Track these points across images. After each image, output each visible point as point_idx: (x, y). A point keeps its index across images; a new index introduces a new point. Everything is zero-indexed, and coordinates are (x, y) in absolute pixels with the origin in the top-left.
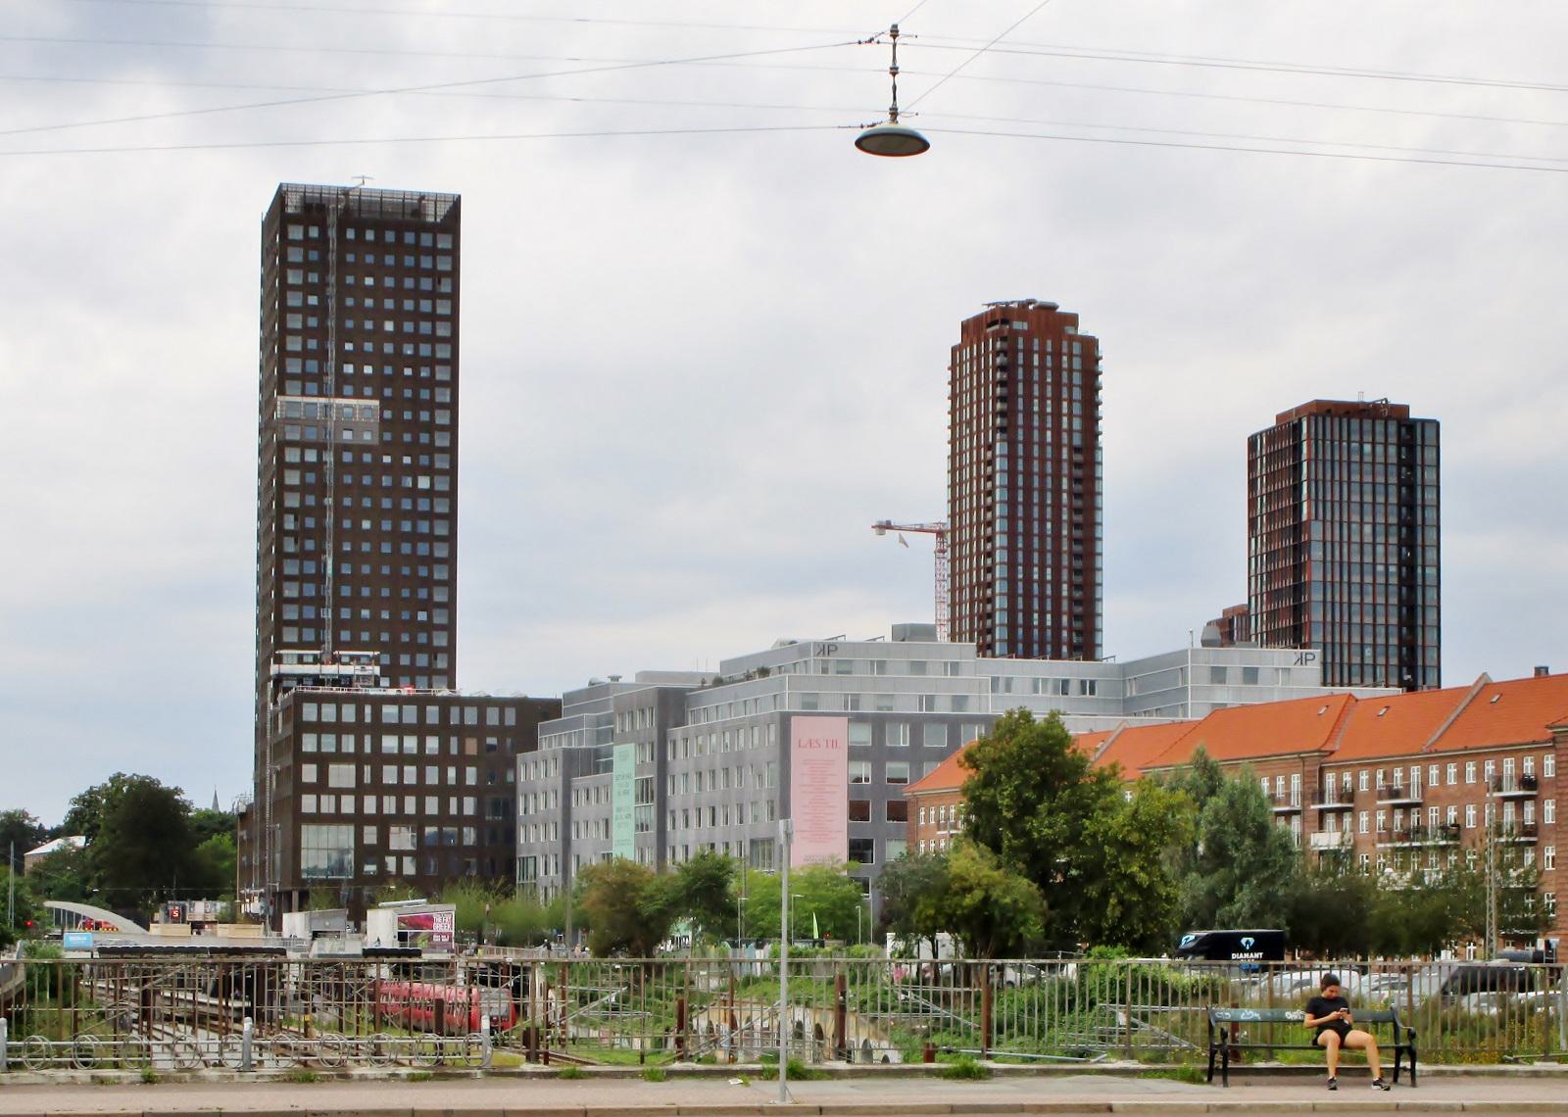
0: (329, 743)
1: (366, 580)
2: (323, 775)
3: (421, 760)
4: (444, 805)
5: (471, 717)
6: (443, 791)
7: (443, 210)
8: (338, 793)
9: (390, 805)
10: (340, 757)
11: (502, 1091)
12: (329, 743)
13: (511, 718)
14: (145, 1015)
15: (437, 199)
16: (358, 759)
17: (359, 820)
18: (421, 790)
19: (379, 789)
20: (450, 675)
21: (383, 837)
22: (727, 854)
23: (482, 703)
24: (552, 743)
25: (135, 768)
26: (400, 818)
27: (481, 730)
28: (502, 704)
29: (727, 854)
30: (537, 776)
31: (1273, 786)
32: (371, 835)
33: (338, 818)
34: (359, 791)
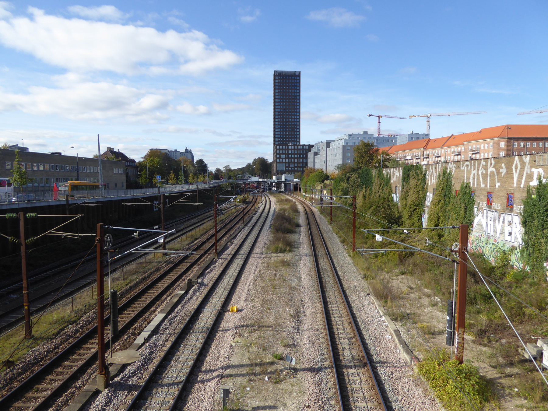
0: (281, 152)
1: (287, 128)
2: (280, 156)
3: (282, 149)
4: (298, 160)
5: (301, 147)
6: (297, 158)
7: (298, 73)
8: (282, 159)
9: (290, 161)
10: (283, 154)
11: (210, 303)
12: (281, 152)
13: (307, 147)
14: (366, 164)
15: (297, 72)
16: (285, 154)
17: (285, 163)
18: (294, 158)
19: (288, 158)
20: (299, 141)
21: (289, 165)
22: (220, 331)
23: (304, 145)
24: (313, 150)
25: (261, 156)
26: (291, 162)
27: (303, 149)
28: (306, 145)
29: (220, 331)
30: (310, 155)
31: (484, 147)
32: (287, 165)
33: (282, 162)
34: (285, 159)
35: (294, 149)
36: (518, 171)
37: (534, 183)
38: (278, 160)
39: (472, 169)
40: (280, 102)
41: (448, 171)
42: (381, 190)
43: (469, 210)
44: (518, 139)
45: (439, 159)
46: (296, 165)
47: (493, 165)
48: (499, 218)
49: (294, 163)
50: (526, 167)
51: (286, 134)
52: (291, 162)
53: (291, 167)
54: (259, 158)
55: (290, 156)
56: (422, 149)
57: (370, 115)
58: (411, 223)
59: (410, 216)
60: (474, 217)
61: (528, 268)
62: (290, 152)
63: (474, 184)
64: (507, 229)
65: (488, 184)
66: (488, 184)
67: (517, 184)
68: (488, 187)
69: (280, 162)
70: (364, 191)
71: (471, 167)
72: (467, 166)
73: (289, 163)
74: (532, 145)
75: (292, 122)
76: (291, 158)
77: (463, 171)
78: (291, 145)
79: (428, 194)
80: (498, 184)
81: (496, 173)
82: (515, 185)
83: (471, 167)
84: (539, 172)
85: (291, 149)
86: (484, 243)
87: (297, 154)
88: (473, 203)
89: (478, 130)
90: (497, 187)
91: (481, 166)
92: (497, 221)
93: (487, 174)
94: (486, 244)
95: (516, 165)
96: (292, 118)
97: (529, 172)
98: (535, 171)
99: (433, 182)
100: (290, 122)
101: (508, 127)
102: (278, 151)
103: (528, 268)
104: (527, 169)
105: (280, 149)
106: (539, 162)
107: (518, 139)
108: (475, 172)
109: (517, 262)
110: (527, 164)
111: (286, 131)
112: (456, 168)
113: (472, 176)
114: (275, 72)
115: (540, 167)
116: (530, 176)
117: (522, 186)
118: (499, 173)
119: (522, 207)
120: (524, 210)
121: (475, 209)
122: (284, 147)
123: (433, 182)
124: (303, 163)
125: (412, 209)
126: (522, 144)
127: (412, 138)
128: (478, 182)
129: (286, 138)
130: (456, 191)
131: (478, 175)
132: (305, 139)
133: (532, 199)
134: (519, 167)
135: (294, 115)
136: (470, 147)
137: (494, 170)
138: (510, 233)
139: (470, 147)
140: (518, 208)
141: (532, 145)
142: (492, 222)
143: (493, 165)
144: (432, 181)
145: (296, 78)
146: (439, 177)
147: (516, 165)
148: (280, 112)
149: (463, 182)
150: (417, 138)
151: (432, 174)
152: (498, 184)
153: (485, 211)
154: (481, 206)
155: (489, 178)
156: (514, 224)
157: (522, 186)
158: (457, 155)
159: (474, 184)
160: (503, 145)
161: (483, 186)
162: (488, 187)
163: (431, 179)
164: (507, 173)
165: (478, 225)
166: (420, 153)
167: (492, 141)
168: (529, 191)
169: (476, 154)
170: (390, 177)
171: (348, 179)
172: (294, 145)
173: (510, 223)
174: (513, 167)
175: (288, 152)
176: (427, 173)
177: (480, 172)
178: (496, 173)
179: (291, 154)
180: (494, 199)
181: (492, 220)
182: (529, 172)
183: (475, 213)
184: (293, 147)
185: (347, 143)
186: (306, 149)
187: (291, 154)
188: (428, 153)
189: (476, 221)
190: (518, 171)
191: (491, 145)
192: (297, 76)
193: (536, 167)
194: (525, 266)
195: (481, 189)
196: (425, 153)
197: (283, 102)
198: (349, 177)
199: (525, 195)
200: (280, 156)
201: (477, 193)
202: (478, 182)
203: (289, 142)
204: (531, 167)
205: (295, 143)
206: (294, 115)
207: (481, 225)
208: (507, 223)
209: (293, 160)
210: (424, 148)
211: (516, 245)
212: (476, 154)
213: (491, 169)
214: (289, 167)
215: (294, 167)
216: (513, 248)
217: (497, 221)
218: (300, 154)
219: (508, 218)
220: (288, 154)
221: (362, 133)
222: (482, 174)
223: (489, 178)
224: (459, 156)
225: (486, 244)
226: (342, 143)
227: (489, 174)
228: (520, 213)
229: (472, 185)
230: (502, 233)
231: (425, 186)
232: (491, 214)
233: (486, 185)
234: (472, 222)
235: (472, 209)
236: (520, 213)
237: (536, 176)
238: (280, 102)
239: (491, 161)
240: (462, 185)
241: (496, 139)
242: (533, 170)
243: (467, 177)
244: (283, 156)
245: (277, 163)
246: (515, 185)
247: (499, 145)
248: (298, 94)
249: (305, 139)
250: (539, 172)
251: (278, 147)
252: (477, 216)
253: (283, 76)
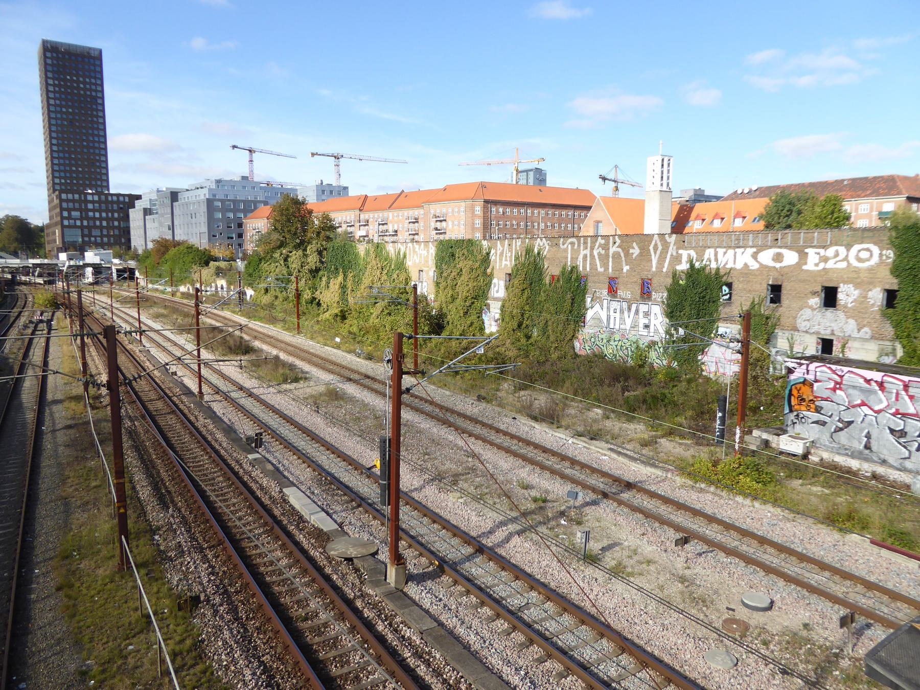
0: (71, 205)
2: (70, 214)
3: (73, 201)
6: (107, 219)
8: (75, 220)
9: (91, 223)
10: (75, 209)
12: (71, 205)
13: (127, 199)
15: (94, 49)
16: (80, 210)
17: (82, 227)
19: (88, 218)
20: (108, 187)
21: (90, 232)
23: (118, 195)
26: (95, 227)
28: (124, 195)
30: (135, 215)
33: (75, 227)
34: (81, 219)
35: (100, 202)
36: (658, 252)
37: (684, 266)
38: (66, 223)
39: (582, 248)
40: (61, 106)
41: (536, 251)
42: (384, 277)
43: (578, 299)
44: (496, 203)
45: (385, 227)
46: (105, 232)
47: (617, 244)
48: (629, 309)
49: (101, 228)
50: (671, 248)
51: (77, 172)
52: (95, 227)
53: (95, 237)
54: (7, 216)
55: (91, 214)
56: (357, 212)
57: (234, 147)
58: (469, 322)
59: (466, 313)
60: (587, 309)
61: (675, 364)
62: (90, 206)
63: (584, 267)
64: (642, 321)
65: (666, 265)
66: (666, 265)
67: (657, 268)
68: (610, 270)
69: (69, 227)
70: (340, 278)
71: (579, 245)
72: (572, 244)
73: (88, 227)
74: (512, 212)
75: (88, 147)
76: (94, 219)
77: (566, 250)
78: (92, 194)
79: (495, 281)
80: (626, 268)
81: (622, 255)
82: (654, 269)
83: (579, 245)
84: (689, 255)
85: (93, 202)
86: (605, 341)
87: (107, 211)
88: (584, 292)
89: (442, 187)
90: (625, 270)
91: (597, 244)
92: (626, 313)
93: (607, 255)
94: (608, 341)
95: (656, 245)
96: (88, 141)
97: (674, 254)
98: (684, 254)
99: (506, 265)
100: (84, 147)
101: (483, 185)
102: (65, 205)
103: (675, 364)
104: (672, 250)
105: (68, 201)
106: (690, 243)
107: (496, 203)
108: (588, 252)
109: (657, 359)
110: (672, 245)
111: (77, 165)
112: (551, 246)
113: (581, 258)
114: (45, 43)
115: (692, 248)
116: (677, 259)
117: (664, 270)
118: (627, 254)
119: (665, 295)
120: (669, 298)
121: (589, 300)
122: (77, 196)
123: (506, 265)
124: (119, 227)
125: (468, 304)
126: (501, 210)
127: (323, 192)
128: (593, 264)
129: (77, 178)
130: (553, 276)
131: (592, 256)
132: (119, 182)
133: (680, 285)
134: (660, 248)
135: (93, 135)
136: (432, 212)
137: (620, 250)
138: (647, 327)
139: (432, 212)
140: (659, 295)
141: (512, 212)
142: (618, 315)
143: (617, 244)
144: (504, 263)
145: (92, 61)
146: (517, 258)
147: (656, 245)
148: (62, 125)
149: (566, 264)
150: (331, 192)
151: (502, 254)
152: (626, 268)
153: (605, 302)
154: (598, 294)
155: (611, 259)
156: (652, 315)
157: (664, 270)
158: (414, 223)
159: (584, 267)
160: (478, 210)
161: (601, 270)
162: (610, 270)
163: (501, 260)
164: (641, 255)
165: (593, 318)
166: (353, 217)
167: (463, 204)
168: (675, 275)
169: (441, 221)
170: (405, 257)
171: (286, 260)
172: (97, 193)
173: (647, 314)
174: (651, 248)
175: (86, 206)
176: (493, 251)
177: (595, 252)
178: (622, 255)
179: (94, 210)
180: (620, 286)
181: (618, 311)
182: (674, 254)
183: (588, 304)
184: (96, 198)
185: (214, 195)
186: (124, 202)
187: (94, 210)
188: (367, 217)
189: (590, 314)
190: (658, 252)
191: (462, 209)
192: (94, 58)
193: (686, 248)
194: (670, 362)
195: (598, 274)
196: (362, 216)
197: (67, 107)
198: (288, 256)
199: (669, 281)
200: (70, 214)
201: (590, 279)
202: (593, 264)
203: (86, 186)
204: (678, 248)
205: (99, 190)
206: (93, 135)
207: (600, 320)
208: (641, 314)
209: (98, 223)
210: (360, 210)
211: (656, 339)
212: (441, 221)
213: (613, 250)
214: (90, 236)
215: (102, 236)
216: (652, 344)
217: (626, 313)
218: (113, 211)
219: (643, 308)
220: (88, 210)
221: (239, 179)
222: (599, 254)
223: (611, 259)
224: (416, 224)
225: (608, 341)
226: (203, 195)
227: (611, 255)
228: (663, 302)
229: (581, 269)
230: (634, 326)
231: (489, 271)
232: (615, 305)
233: (607, 269)
234: (584, 316)
235: (583, 300)
236: (663, 302)
237: (685, 259)
238: (61, 106)
239: (614, 239)
240: (564, 268)
241: (469, 202)
242: (680, 252)
243: (572, 258)
244: (76, 214)
245: (63, 227)
246: (654, 269)
247: (473, 211)
248: (99, 95)
249: (119, 182)
250: (689, 255)
251: (64, 196)
252: (592, 308)
253: (64, 53)
